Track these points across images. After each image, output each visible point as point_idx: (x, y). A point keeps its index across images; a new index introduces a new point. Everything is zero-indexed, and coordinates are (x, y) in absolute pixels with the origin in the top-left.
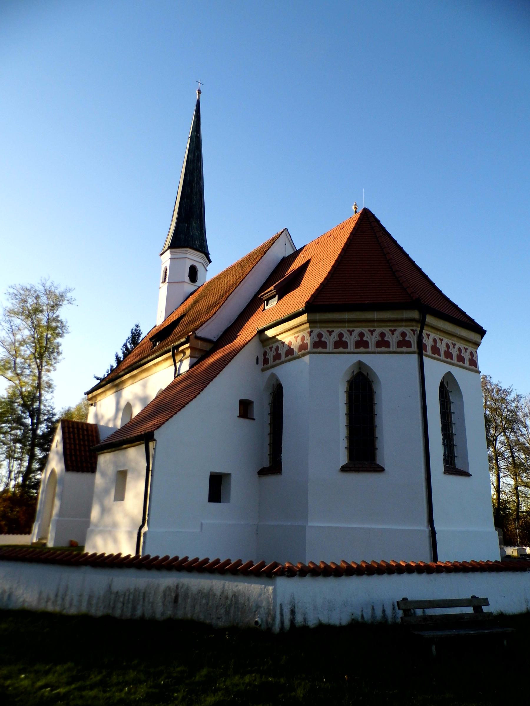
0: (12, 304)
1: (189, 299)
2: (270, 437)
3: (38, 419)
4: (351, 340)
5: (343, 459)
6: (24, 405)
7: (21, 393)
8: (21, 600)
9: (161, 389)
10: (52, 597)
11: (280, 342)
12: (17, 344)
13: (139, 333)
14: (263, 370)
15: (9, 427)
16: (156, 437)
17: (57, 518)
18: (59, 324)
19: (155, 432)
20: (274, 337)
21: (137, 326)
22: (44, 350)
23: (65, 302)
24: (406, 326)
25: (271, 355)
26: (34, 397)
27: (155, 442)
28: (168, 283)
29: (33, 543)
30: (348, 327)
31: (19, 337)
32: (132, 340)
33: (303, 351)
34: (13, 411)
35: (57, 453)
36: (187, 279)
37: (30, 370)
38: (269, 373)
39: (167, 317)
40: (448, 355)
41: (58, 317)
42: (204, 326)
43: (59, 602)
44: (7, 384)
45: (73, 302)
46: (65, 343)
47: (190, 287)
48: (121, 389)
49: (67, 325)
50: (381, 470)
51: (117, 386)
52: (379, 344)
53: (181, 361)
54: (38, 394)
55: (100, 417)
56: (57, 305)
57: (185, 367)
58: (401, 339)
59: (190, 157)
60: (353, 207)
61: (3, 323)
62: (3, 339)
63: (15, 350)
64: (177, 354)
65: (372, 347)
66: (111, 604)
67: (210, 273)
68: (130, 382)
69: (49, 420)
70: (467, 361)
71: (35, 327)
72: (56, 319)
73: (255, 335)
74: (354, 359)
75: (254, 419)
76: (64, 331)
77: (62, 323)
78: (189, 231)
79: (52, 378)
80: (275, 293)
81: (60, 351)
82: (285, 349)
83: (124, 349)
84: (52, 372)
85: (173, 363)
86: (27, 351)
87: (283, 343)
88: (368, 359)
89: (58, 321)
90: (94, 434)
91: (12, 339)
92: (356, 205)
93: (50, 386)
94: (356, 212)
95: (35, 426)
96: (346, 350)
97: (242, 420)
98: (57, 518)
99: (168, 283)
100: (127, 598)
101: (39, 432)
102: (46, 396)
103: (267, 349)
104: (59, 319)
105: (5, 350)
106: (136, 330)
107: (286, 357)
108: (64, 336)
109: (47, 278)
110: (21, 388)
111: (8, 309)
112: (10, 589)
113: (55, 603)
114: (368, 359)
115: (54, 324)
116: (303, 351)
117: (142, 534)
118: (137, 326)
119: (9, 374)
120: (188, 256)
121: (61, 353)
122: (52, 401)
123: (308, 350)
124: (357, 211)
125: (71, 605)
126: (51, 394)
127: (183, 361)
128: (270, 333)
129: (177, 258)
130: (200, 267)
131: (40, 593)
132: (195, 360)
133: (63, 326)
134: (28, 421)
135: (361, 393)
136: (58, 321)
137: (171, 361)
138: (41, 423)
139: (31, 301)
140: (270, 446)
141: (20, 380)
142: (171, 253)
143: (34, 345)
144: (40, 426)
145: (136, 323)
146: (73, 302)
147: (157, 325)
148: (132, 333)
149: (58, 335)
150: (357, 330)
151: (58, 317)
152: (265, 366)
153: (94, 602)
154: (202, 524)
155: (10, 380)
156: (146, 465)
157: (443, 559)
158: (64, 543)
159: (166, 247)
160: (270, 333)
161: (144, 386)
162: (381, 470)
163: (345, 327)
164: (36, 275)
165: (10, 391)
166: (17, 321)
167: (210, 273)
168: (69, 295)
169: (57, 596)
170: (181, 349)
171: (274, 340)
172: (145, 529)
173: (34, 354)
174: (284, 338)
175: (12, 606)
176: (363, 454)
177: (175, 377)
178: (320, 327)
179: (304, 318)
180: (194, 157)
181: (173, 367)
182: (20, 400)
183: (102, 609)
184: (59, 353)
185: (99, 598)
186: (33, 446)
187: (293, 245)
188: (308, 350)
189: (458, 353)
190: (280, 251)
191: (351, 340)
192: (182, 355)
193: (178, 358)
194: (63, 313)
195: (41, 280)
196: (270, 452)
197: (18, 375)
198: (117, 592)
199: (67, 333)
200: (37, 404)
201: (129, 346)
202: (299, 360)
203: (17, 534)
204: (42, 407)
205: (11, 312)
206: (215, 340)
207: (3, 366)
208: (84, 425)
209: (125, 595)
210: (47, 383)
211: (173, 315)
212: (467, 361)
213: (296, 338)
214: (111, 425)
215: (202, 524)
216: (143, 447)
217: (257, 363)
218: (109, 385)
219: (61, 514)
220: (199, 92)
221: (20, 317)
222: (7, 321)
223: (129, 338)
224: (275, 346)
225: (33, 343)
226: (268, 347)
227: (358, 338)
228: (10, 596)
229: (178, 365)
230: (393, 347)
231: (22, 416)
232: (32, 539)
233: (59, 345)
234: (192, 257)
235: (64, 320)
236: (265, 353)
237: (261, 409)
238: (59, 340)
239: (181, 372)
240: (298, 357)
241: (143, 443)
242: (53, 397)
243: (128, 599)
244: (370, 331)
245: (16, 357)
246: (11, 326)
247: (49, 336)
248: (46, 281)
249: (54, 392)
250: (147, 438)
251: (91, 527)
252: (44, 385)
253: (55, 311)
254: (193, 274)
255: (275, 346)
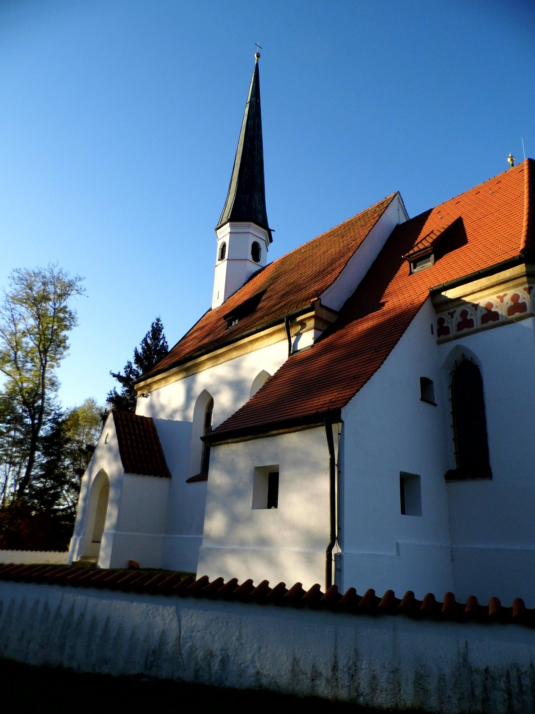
0: (15, 289)
1: (255, 279)
2: (454, 430)
3: (40, 419)
5: (453, 466)
6: (25, 403)
7: (21, 389)
8: (252, 671)
9: (263, 372)
10: (326, 671)
11: (470, 305)
12: (18, 335)
13: (160, 328)
14: (439, 343)
15: (6, 427)
16: (343, 416)
17: (113, 532)
18: (67, 316)
19: (343, 410)
20: (459, 299)
21: (158, 320)
22: (50, 341)
23: (74, 292)
25: (452, 323)
26: (37, 394)
27: (340, 424)
28: (227, 260)
29: (74, 564)
31: (21, 326)
33: (517, 314)
34: (13, 410)
35: (110, 449)
36: (250, 257)
37: (33, 364)
38: (450, 346)
39: (227, 298)
41: (65, 307)
42: (325, 292)
43: (344, 679)
44: (6, 379)
45: (83, 293)
46: (72, 336)
47: (253, 267)
48: (196, 373)
49: (77, 316)
51: (187, 370)
53: (299, 335)
54: (40, 392)
55: (158, 407)
56: (65, 294)
57: (307, 340)
59: (249, 122)
60: (509, 160)
61: (3, 311)
62: (3, 328)
63: (16, 341)
64: (292, 326)
66: (478, 692)
67: (272, 255)
68: (209, 364)
69: (54, 421)
71: (39, 317)
72: (64, 310)
73: (428, 297)
75: (436, 405)
76: (72, 323)
77: (71, 314)
78: (249, 205)
79: (57, 375)
80: (431, 251)
81: (68, 345)
82: (479, 314)
83: (144, 345)
84: (55, 368)
85: (287, 337)
86: (29, 342)
87: (476, 306)
89: (66, 312)
90: (151, 429)
91: (13, 329)
92: (512, 157)
93: (53, 384)
94: (513, 165)
95: (35, 428)
97: (424, 404)
98: (113, 532)
99: (227, 260)
100: (514, 683)
101: (42, 433)
102: (49, 394)
103: (445, 315)
104: (67, 310)
105: (4, 341)
106: (157, 324)
107: (458, 330)
108: (72, 329)
109: (55, 264)
110: (22, 383)
111: (10, 295)
112: (222, 649)
113: (333, 681)
115: (61, 315)
116: (517, 314)
117: (333, 558)
118: (158, 320)
119: (8, 368)
120: (251, 231)
121: (68, 347)
122: (55, 400)
123: (528, 311)
124: (514, 163)
125: (373, 689)
126: (55, 393)
127: (301, 334)
128: (451, 294)
129: (239, 233)
130: (262, 244)
131: (295, 661)
132: (320, 333)
133: (72, 317)
134: (28, 421)
136: (66, 312)
137: (284, 335)
138: (44, 424)
139: (38, 287)
140: (455, 442)
141: (20, 375)
142: (231, 226)
143: (38, 336)
144: (43, 427)
145: (157, 316)
146: (83, 293)
147: (213, 308)
148: (153, 327)
149: (67, 328)
151: (65, 307)
152: (443, 337)
153: (432, 685)
154: (398, 544)
155: (8, 375)
156: (329, 456)
158: (122, 565)
159: (225, 220)
160: (451, 294)
161: (237, 367)
164: (42, 258)
165: (10, 387)
166: (22, 309)
167: (272, 255)
168: (78, 284)
169: (335, 668)
170: (299, 319)
171: (460, 302)
172: (336, 550)
173: (38, 346)
174: (477, 299)
175: (232, 681)
177: (290, 355)
179: (521, 269)
180: (254, 123)
181: (287, 342)
182: (19, 397)
183: (454, 700)
184: (65, 348)
185: (442, 678)
186: (34, 448)
187: (406, 214)
188: (528, 311)
190: (393, 217)
192: (299, 327)
193: (293, 332)
194: (72, 303)
195: (49, 266)
196: (456, 450)
197: (18, 368)
198: (487, 670)
199: (75, 326)
200: (40, 402)
201: (149, 341)
202: (512, 325)
203: (17, 550)
204: (45, 405)
205: (15, 299)
206: (338, 310)
207: (2, 358)
208: (144, 419)
209: (508, 677)
210: (50, 380)
211: (236, 296)
213: (501, 299)
214: (178, 418)
215: (398, 544)
216: (322, 432)
217: (432, 333)
218: (174, 370)
219: (117, 527)
220: (258, 56)
221: (24, 305)
223: (149, 333)
224: (459, 310)
225: (37, 334)
226: (446, 313)
228: (224, 662)
229: (293, 340)
231: (22, 416)
232: (71, 557)
233: (66, 338)
234: (253, 233)
235: (73, 311)
236: (441, 321)
237: (442, 391)
238: (64, 333)
239: (299, 348)
240: (478, 331)
241: (322, 425)
242: (56, 396)
243: (520, 685)
245: (18, 350)
246: (12, 315)
247: (55, 327)
248: (55, 267)
249: (59, 390)
250: (328, 418)
251: (206, 545)
252: (47, 381)
253: (62, 301)
254: (256, 252)
255: (459, 310)
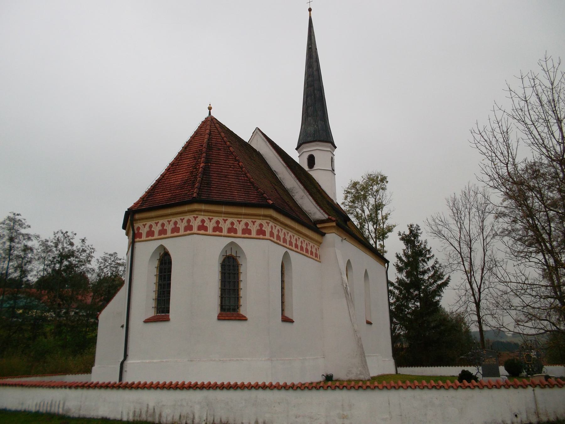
4: (225, 226)
5: (152, 313)
24: (263, 219)
30: (224, 217)
32: (104, 278)
40: (232, 230)
50: (243, 318)
52: (200, 228)
58: (201, 224)
65: (239, 234)
70: (275, 236)
74: (230, 240)
88: (237, 241)
96: (153, 238)
114: (237, 241)
120: (305, 150)
135: (230, 269)
150: (215, 219)
157: (128, 378)
162: (243, 318)
163: (221, 217)
176: (230, 305)
178: (204, 215)
189: (277, 233)
191: (225, 226)
212: (275, 236)
220: (310, 10)
222: (47, 247)
227: (200, 224)
230: (210, 231)
244: (252, 221)
